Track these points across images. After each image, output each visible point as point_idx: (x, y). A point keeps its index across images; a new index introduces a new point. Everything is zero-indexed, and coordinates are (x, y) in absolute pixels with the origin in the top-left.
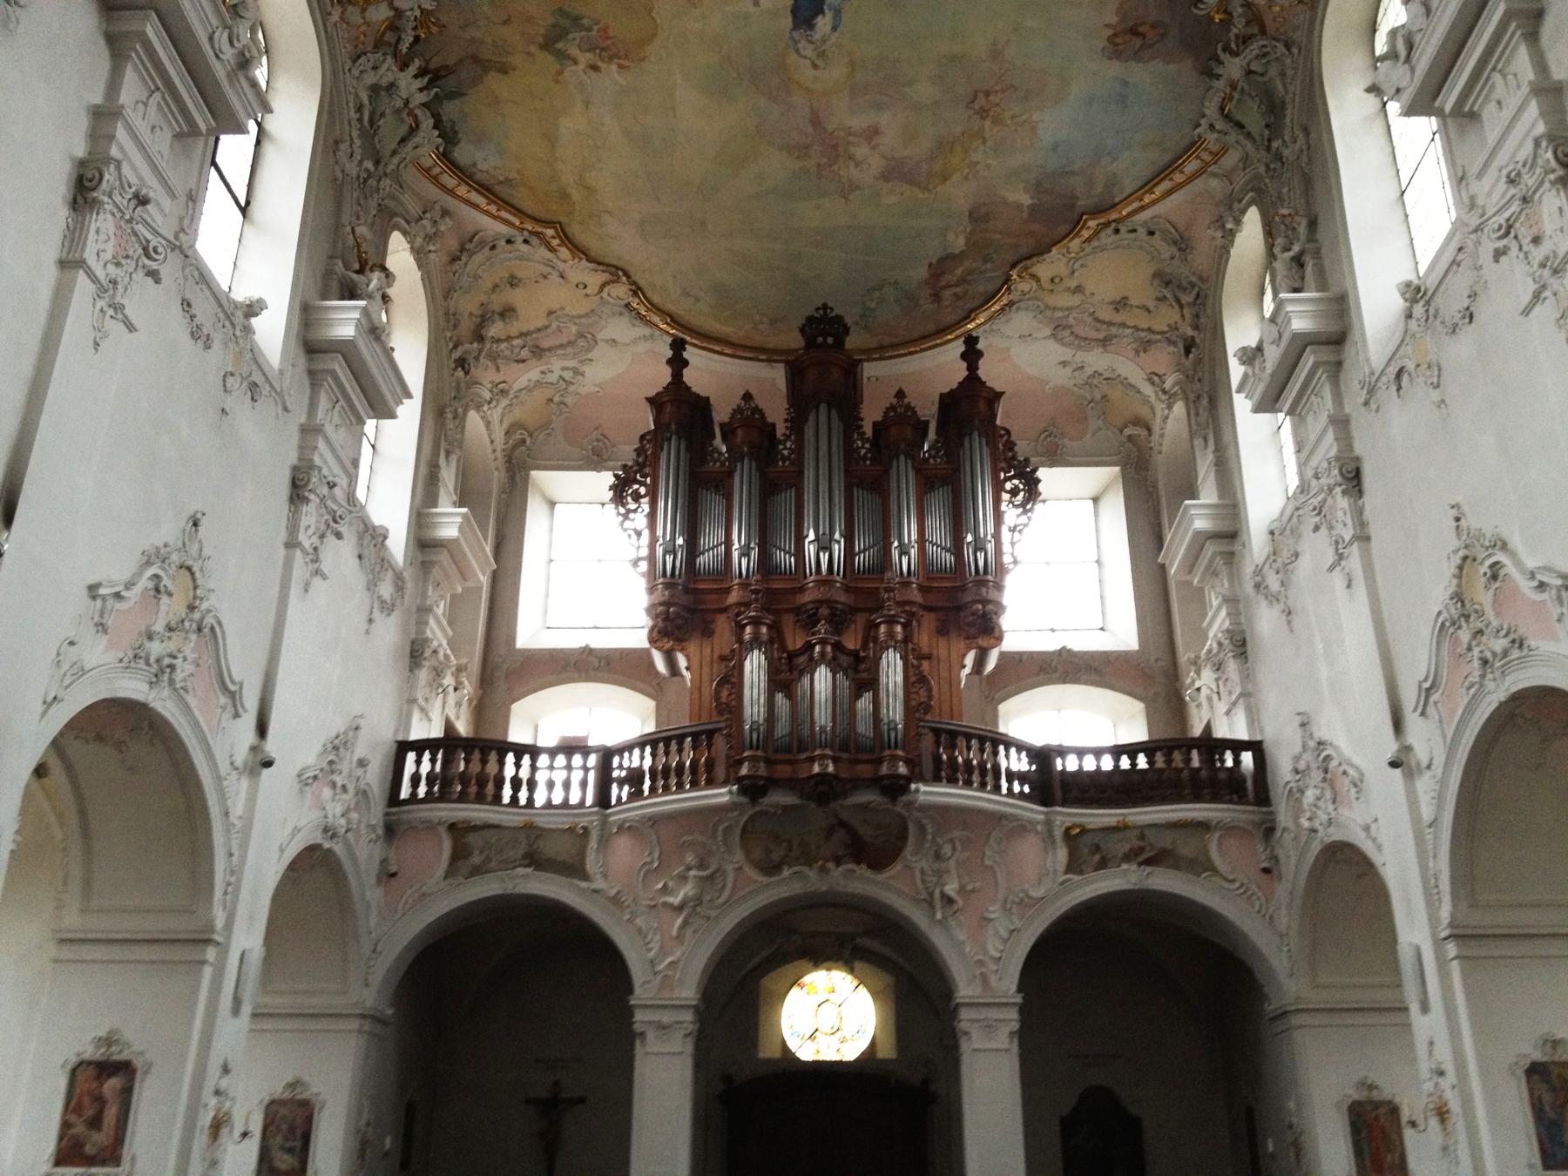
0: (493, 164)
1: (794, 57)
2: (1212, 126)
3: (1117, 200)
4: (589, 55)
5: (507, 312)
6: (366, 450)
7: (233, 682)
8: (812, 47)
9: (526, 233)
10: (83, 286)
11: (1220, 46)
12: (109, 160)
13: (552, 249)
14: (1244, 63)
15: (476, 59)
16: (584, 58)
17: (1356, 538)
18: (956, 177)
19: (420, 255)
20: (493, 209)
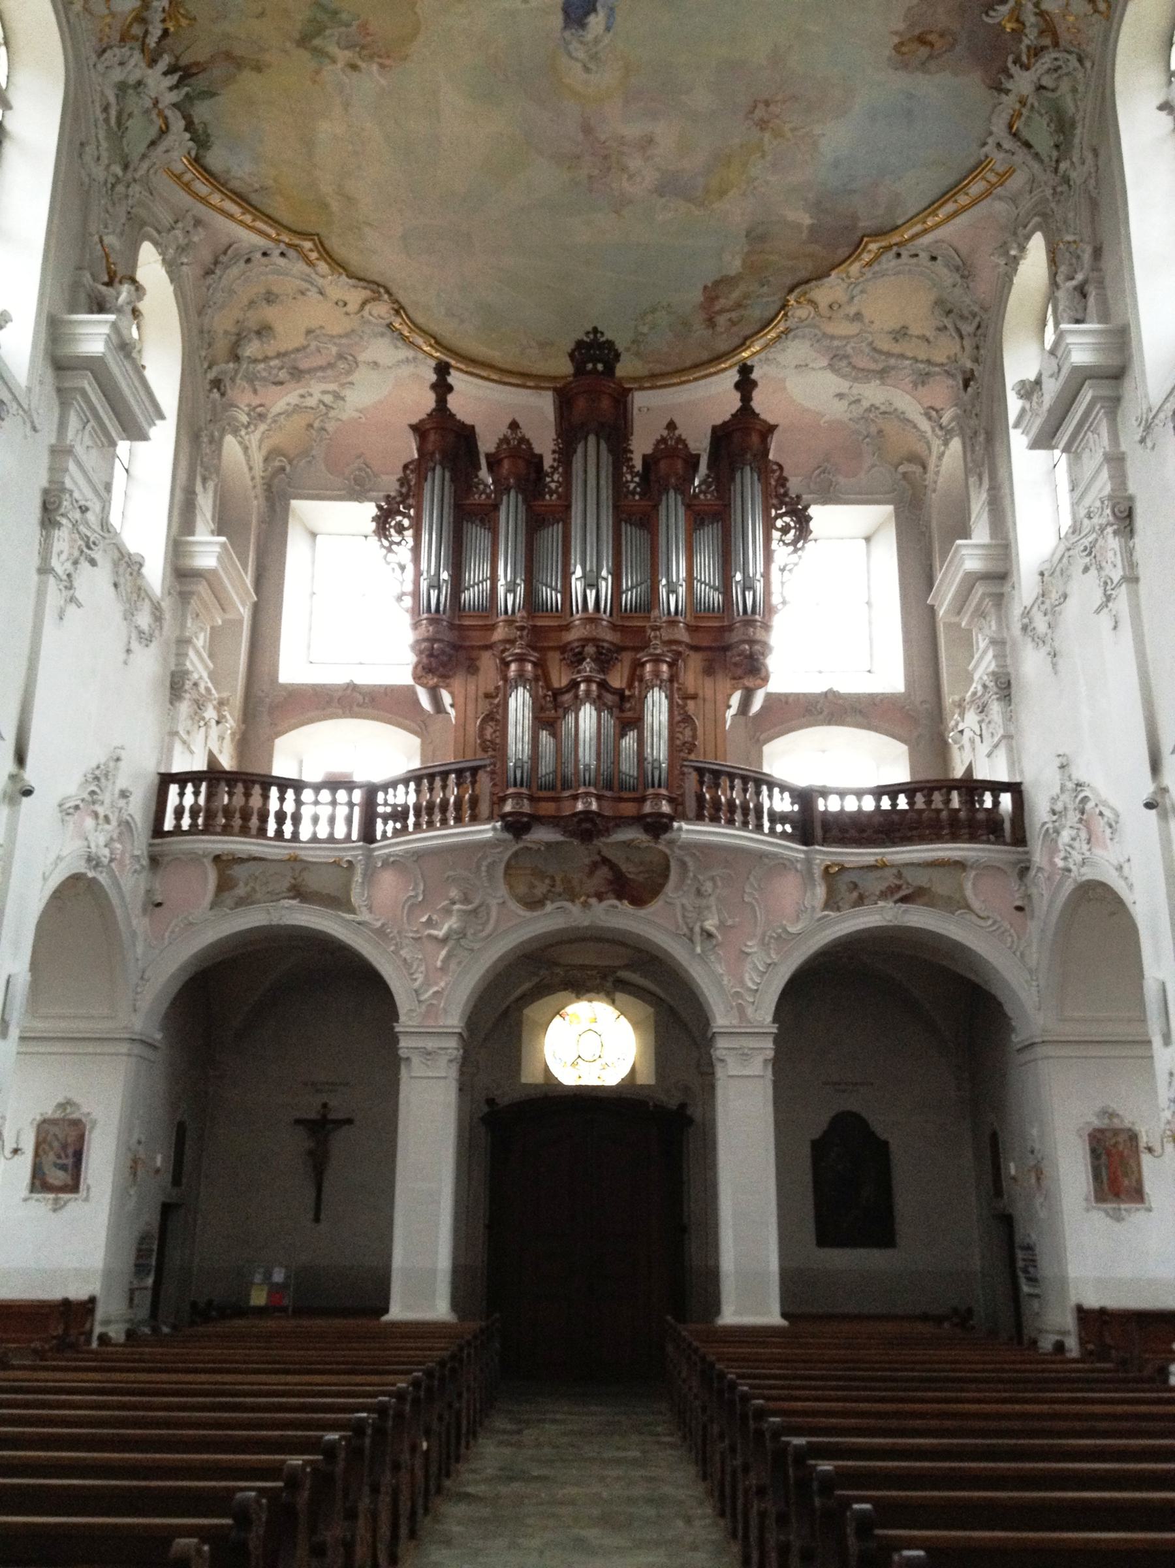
2: (999, 145)
13: (310, 263)
15: (228, 56)
16: (343, 56)
19: (172, 267)
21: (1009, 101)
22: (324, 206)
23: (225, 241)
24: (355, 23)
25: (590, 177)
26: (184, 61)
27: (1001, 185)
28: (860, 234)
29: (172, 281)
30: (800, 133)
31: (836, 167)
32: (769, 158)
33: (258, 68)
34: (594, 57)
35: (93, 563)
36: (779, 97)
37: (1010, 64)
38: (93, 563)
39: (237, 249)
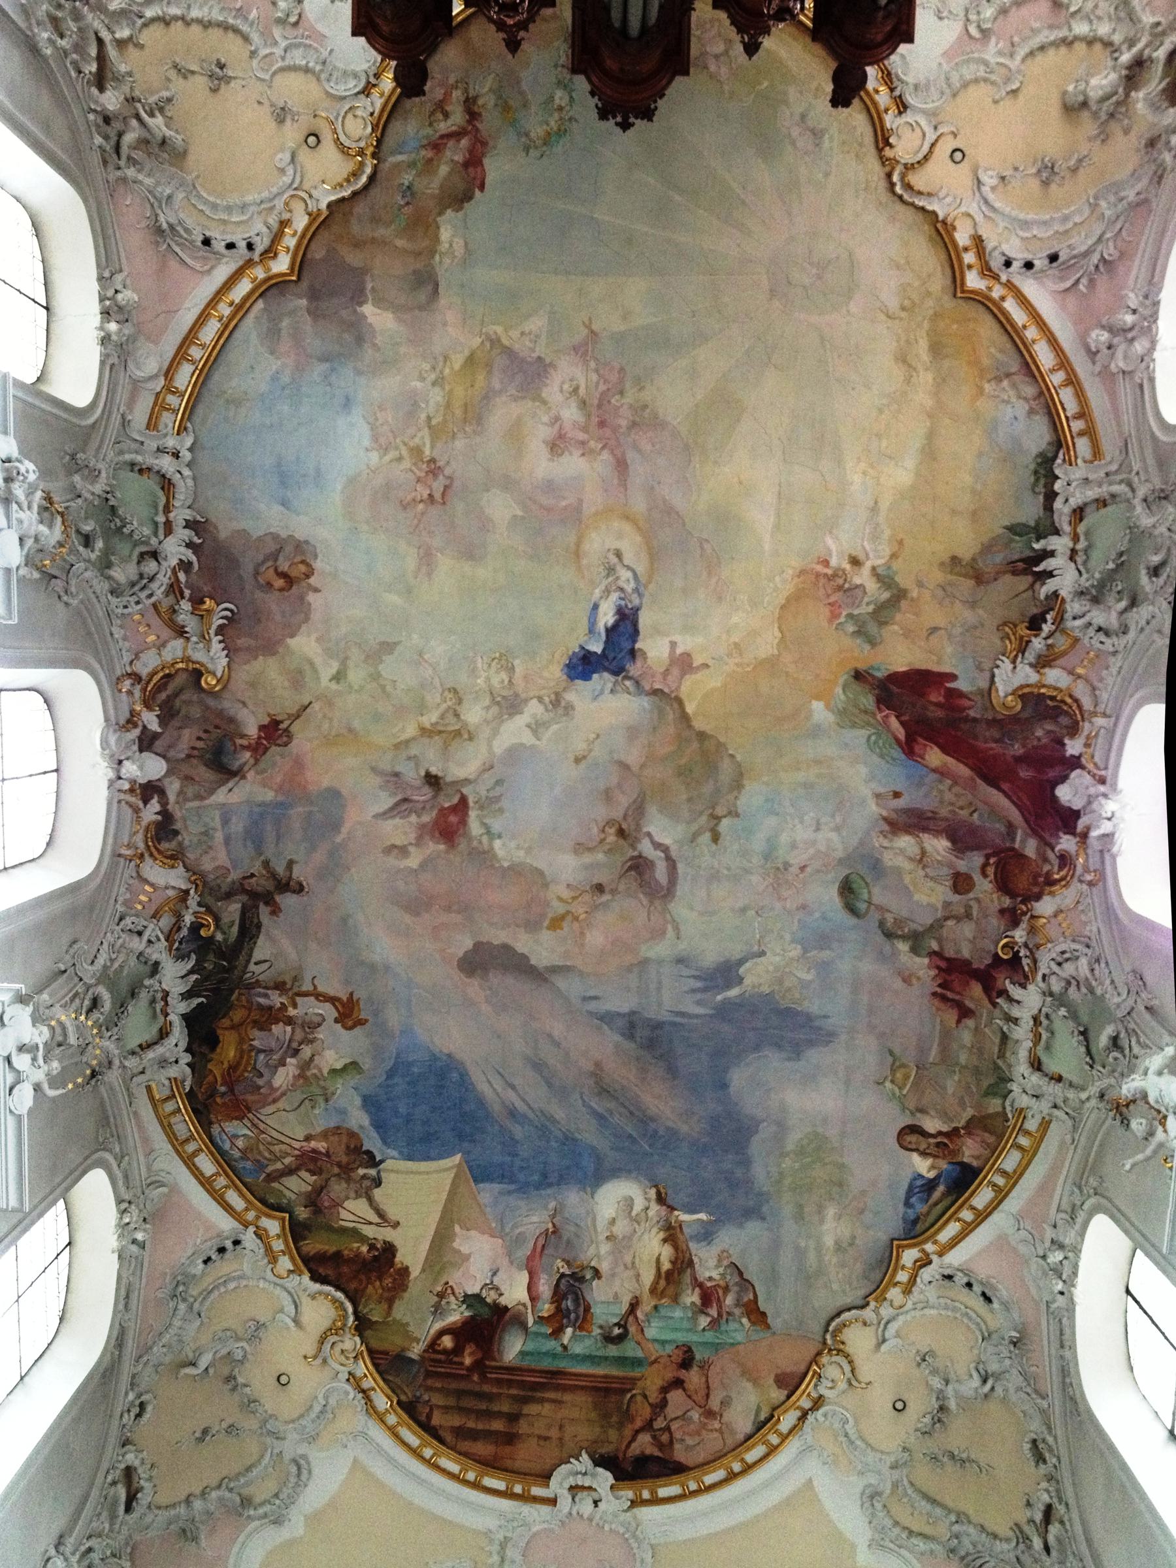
0: (1009, 410)
1: (641, 569)
2: (176, 455)
3: (260, 304)
4: (857, 581)
5: (1074, 108)
8: (621, 583)
9: (1004, 278)
11: (196, 566)
13: (978, 241)
14: (164, 564)
15: (979, 579)
16: (863, 578)
18: (458, 361)
20: (1031, 333)
21: (180, 515)
22: (936, 349)
23: (1071, 301)
24: (842, 619)
25: (621, 393)
26: (1025, 581)
27: (158, 394)
28: (305, 284)
29: (1156, 304)
30: (392, 454)
31: (348, 399)
32: (423, 416)
33: (955, 560)
34: (611, 570)
36: (421, 506)
37: (194, 559)
39: (1062, 279)
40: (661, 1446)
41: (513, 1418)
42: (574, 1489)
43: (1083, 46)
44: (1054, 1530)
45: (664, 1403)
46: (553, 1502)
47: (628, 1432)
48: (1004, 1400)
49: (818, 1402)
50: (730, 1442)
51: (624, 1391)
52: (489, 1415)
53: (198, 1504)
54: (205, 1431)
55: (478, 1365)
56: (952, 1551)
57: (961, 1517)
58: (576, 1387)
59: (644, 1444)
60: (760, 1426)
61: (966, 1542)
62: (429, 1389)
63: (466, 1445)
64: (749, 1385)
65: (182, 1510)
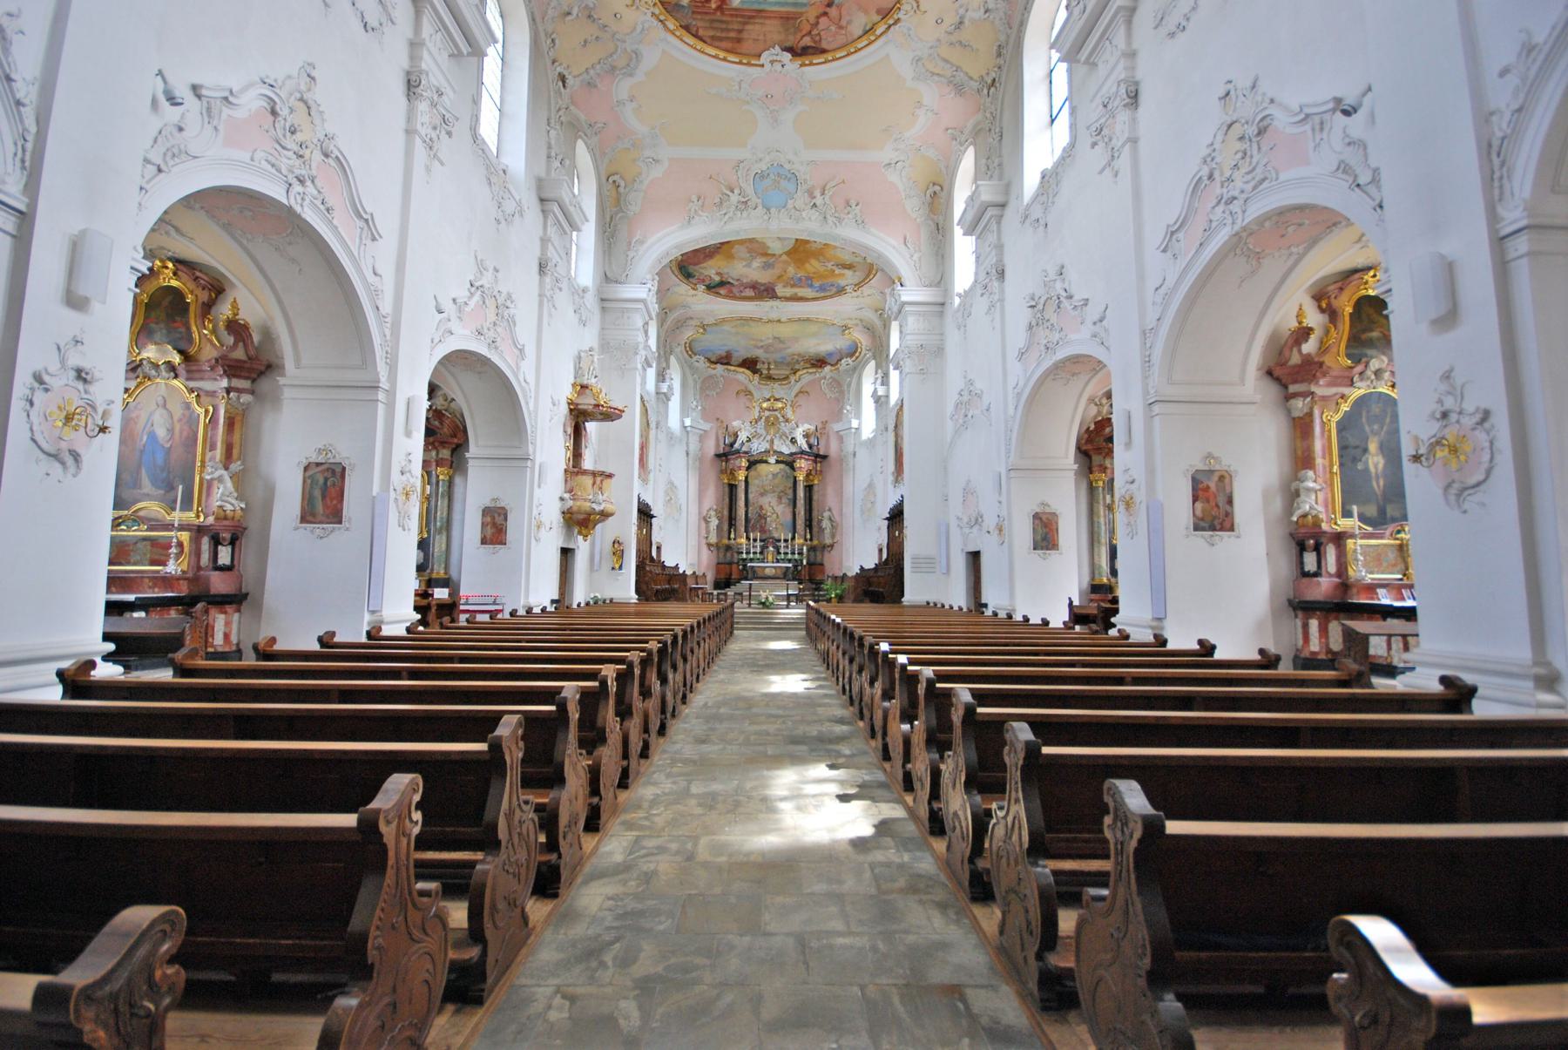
6: (574, 247)
7: (366, 212)
10: (419, 146)
12: (421, 72)
17: (999, 300)
19: (591, 150)
35: (560, 289)
38: (560, 289)
40: (815, 42)
41: (740, 31)
42: (772, 62)
43: (783, 320)
44: (993, 89)
45: (817, 23)
46: (763, 66)
47: (799, 37)
48: (993, 22)
49: (897, 21)
50: (850, 39)
51: (797, 19)
52: (728, 30)
53: (592, 72)
54: (585, 42)
55: (719, 8)
56: (951, 82)
57: (958, 69)
58: (770, 17)
59: (807, 41)
60: (866, 32)
61: (958, 78)
62: (694, 19)
63: (717, 44)
64: (862, 14)
65: (585, 75)
